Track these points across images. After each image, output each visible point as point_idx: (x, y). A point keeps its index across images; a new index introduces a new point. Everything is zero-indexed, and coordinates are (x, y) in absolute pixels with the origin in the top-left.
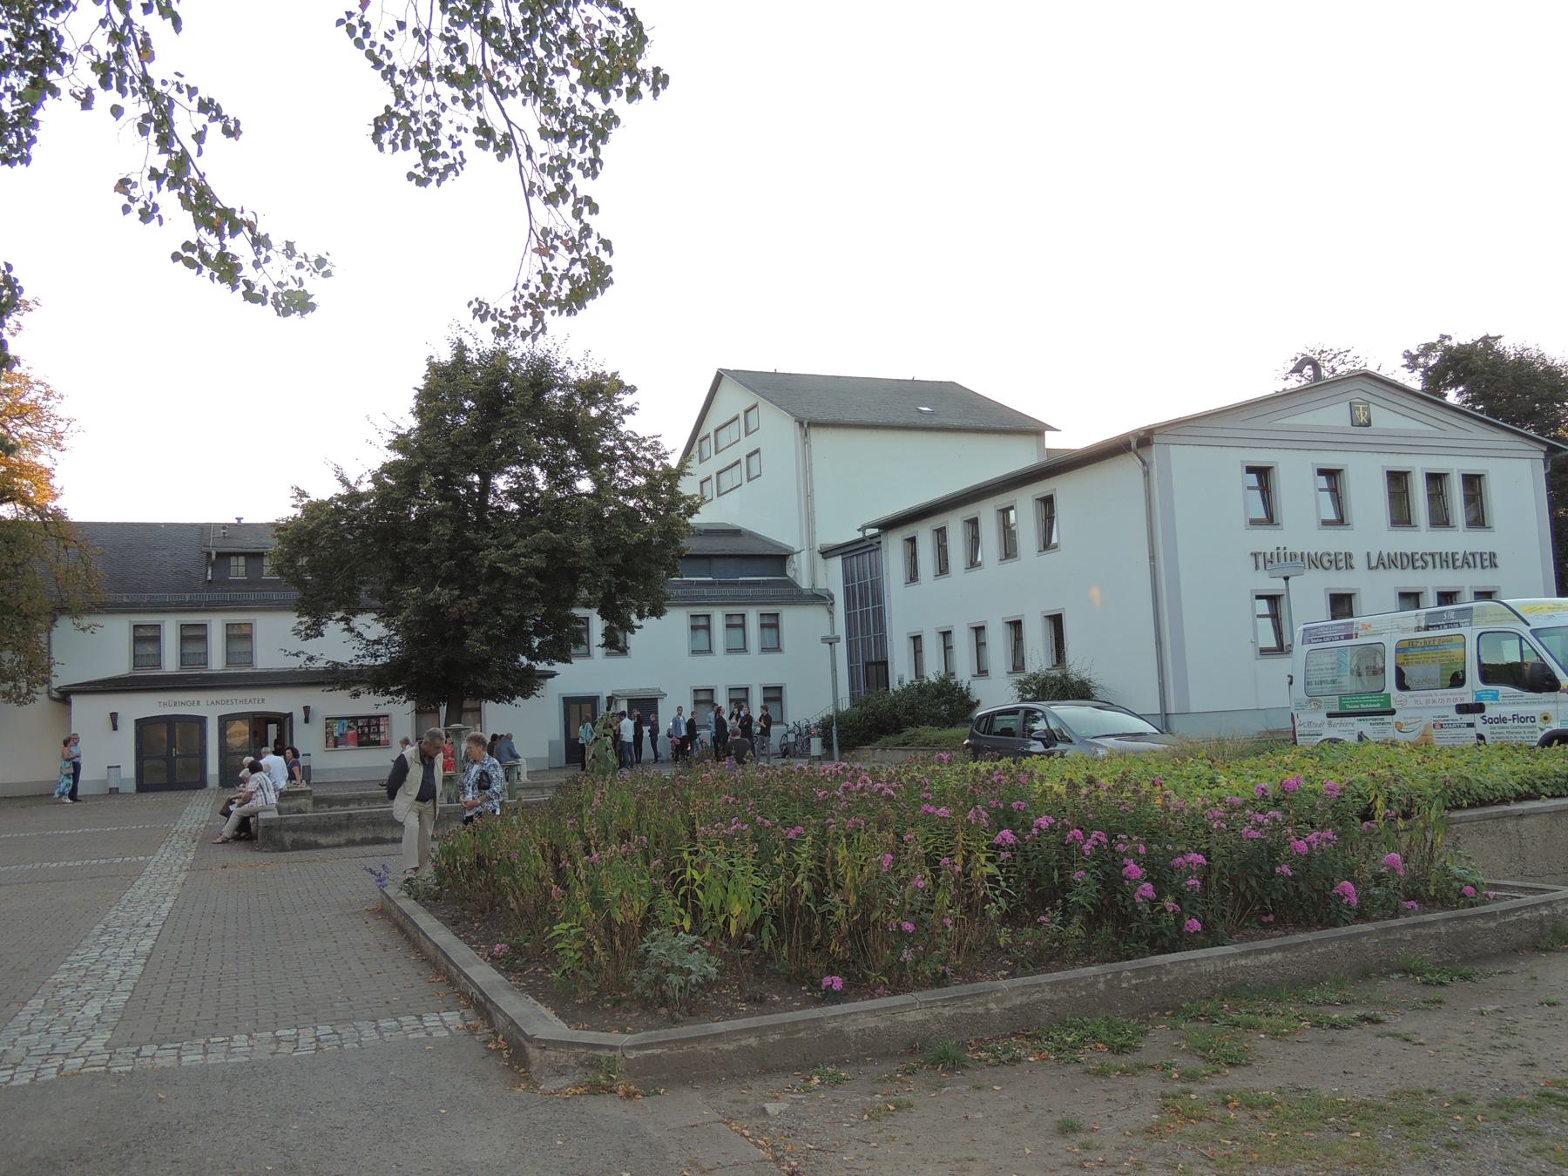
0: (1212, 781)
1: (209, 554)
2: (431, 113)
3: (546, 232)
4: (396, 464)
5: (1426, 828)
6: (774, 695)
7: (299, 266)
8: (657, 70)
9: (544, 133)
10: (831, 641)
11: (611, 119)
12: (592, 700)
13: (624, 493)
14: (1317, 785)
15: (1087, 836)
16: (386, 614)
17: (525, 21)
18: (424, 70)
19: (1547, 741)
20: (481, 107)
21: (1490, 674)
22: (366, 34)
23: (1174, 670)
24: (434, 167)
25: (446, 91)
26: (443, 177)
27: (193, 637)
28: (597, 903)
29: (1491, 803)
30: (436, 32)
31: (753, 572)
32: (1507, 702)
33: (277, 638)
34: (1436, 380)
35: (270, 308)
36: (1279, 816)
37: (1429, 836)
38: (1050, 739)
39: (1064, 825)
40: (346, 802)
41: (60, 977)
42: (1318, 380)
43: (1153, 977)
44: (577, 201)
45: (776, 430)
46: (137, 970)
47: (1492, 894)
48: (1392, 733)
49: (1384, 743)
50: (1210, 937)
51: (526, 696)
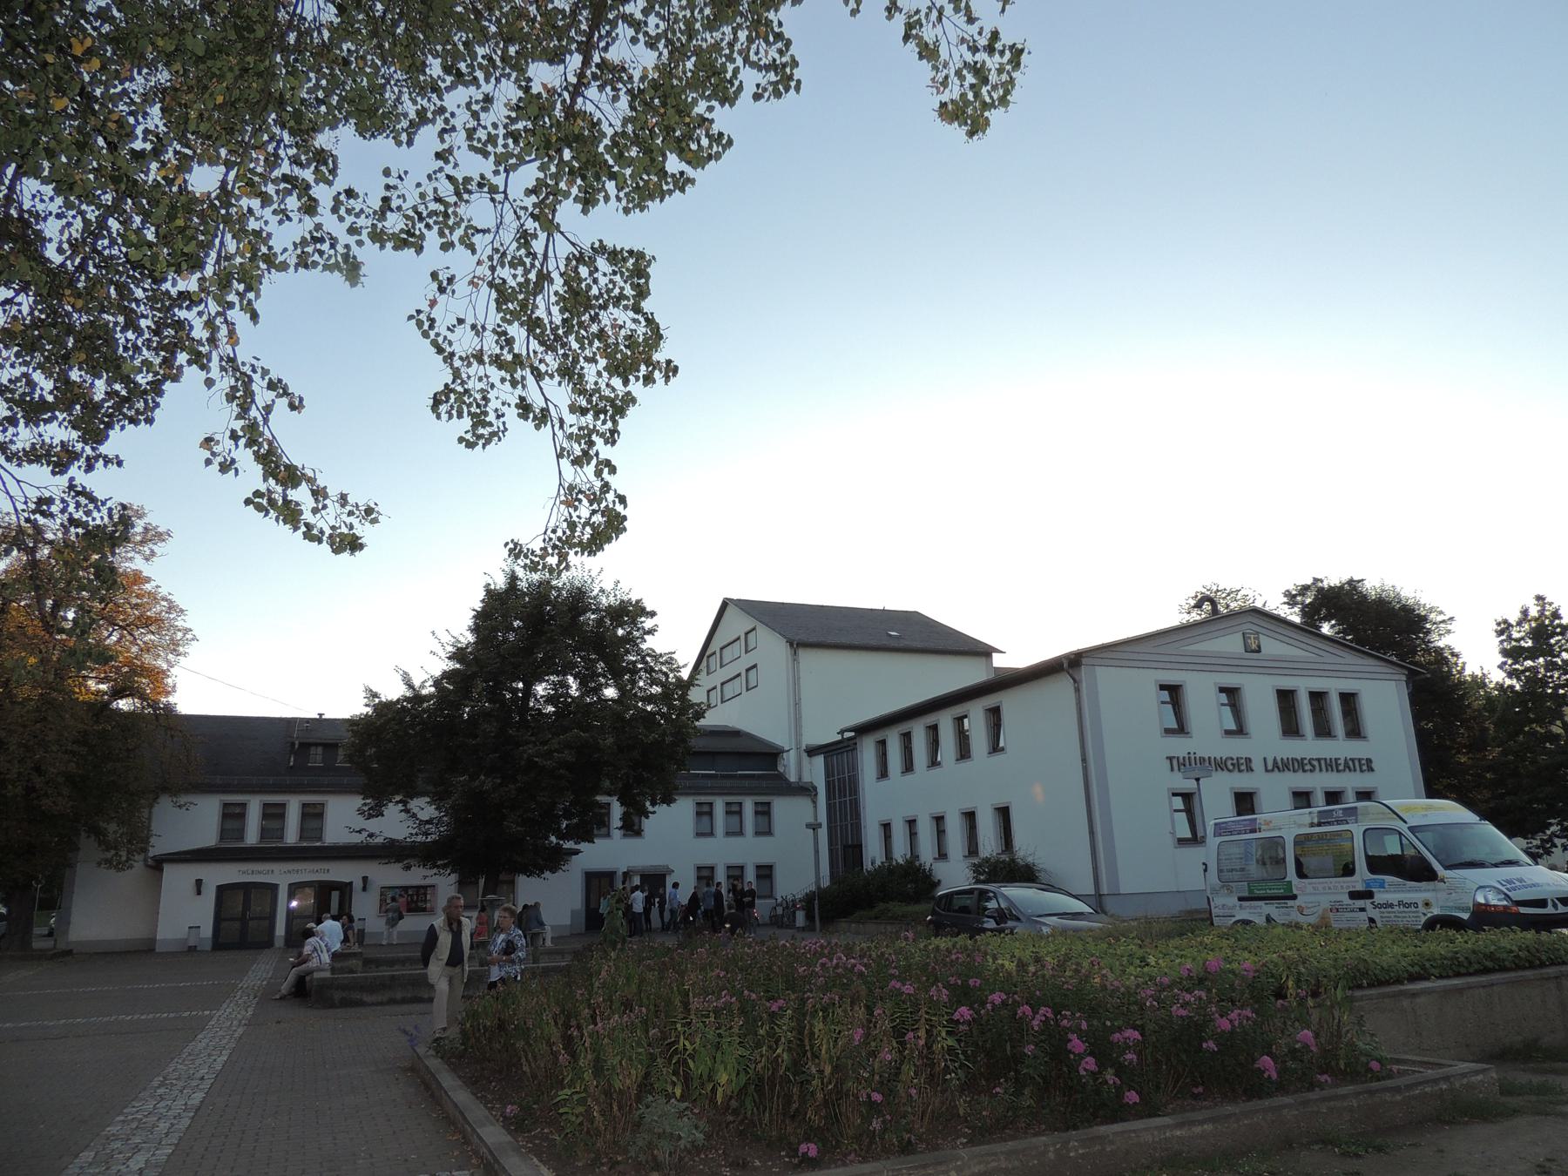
0: (1143, 959)
1: (293, 744)
2: (482, 390)
3: (571, 488)
4: (454, 671)
5: (1332, 1006)
6: (765, 872)
7: (350, 513)
8: (669, 362)
9: (573, 409)
10: (814, 827)
11: (630, 400)
12: (610, 875)
13: (643, 699)
14: (1235, 966)
15: (1035, 1012)
16: (438, 799)
17: (564, 321)
18: (479, 356)
19: (1431, 924)
20: (524, 387)
21: (1378, 865)
22: (431, 327)
23: (1104, 848)
24: (482, 433)
25: (495, 374)
26: (488, 442)
27: (274, 814)
28: (598, 1068)
29: (1387, 983)
30: (489, 327)
31: (750, 766)
32: (1393, 891)
33: (344, 818)
34: (1312, 615)
35: (325, 547)
36: (1203, 995)
37: (1336, 1014)
38: (1001, 916)
39: (1014, 1001)
40: (391, 963)
41: (112, 1129)
42: (1215, 614)
43: (1098, 1147)
44: (599, 463)
45: (771, 647)
46: (186, 1122)
47: (1395, 1068)
48: (1295, 916)
49: (1289, 926)
50: (1149, 1109)
51: (553, 870)
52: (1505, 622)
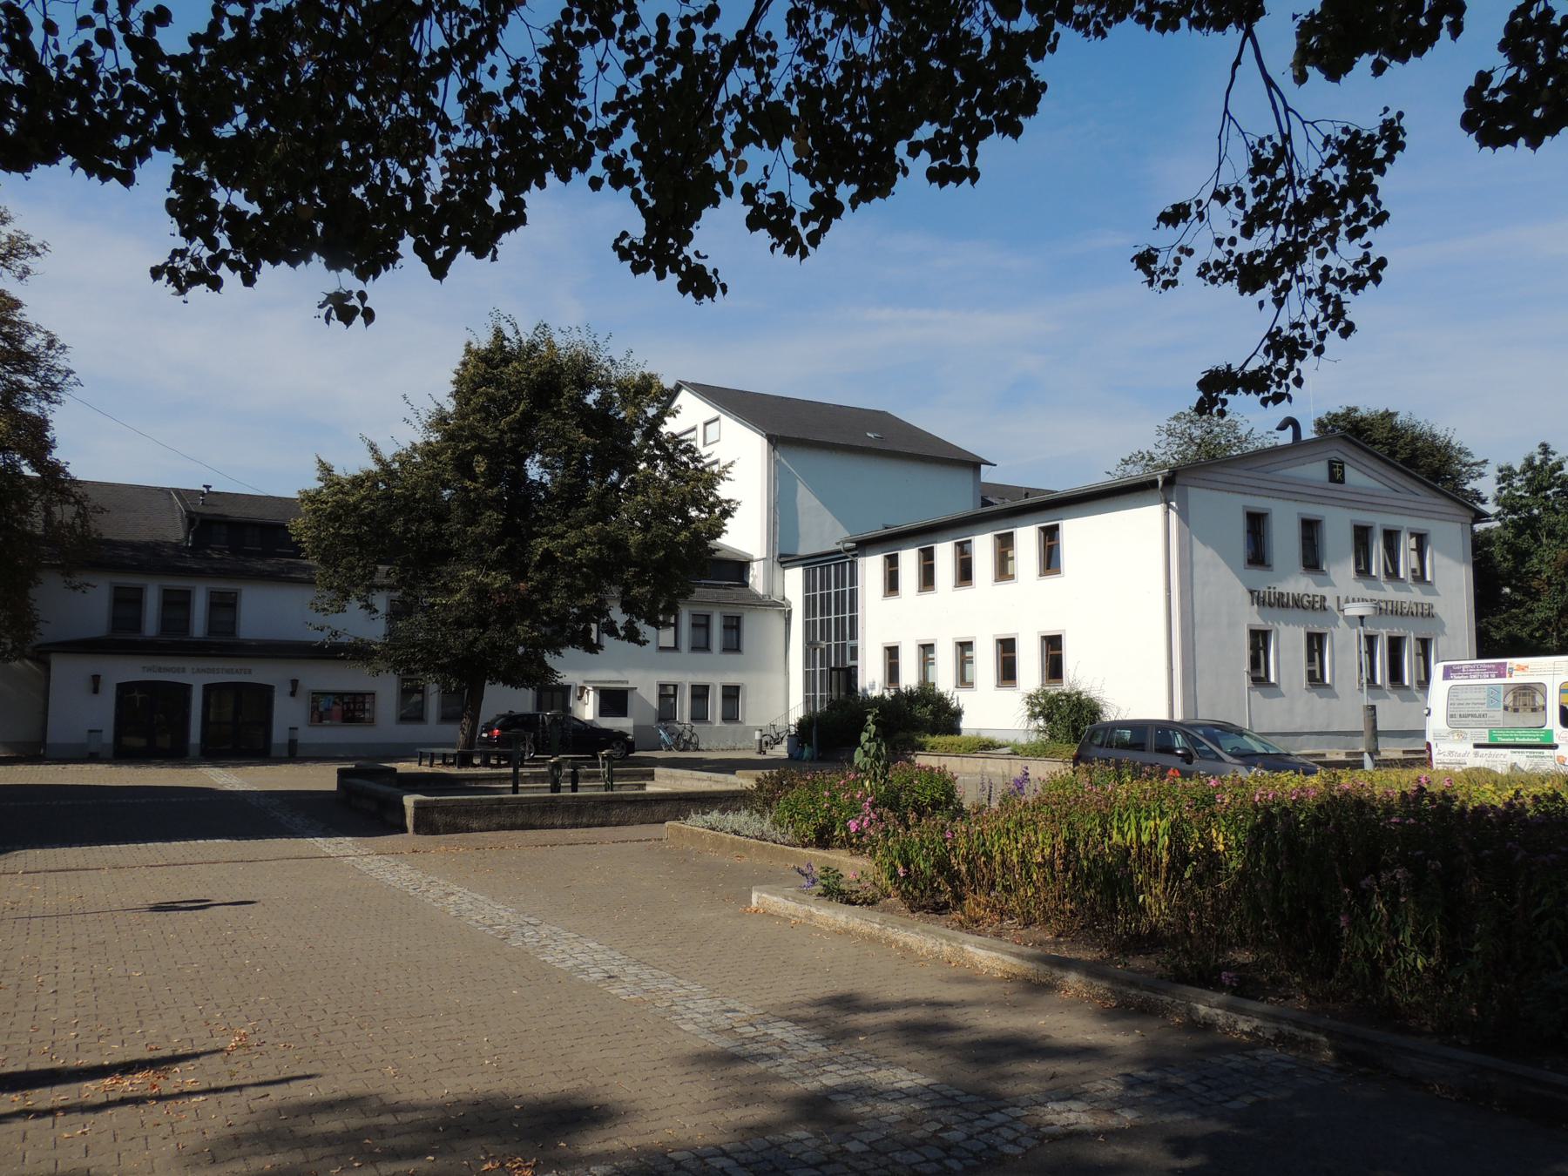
27: (176, 603)
52: (1510, 468)
